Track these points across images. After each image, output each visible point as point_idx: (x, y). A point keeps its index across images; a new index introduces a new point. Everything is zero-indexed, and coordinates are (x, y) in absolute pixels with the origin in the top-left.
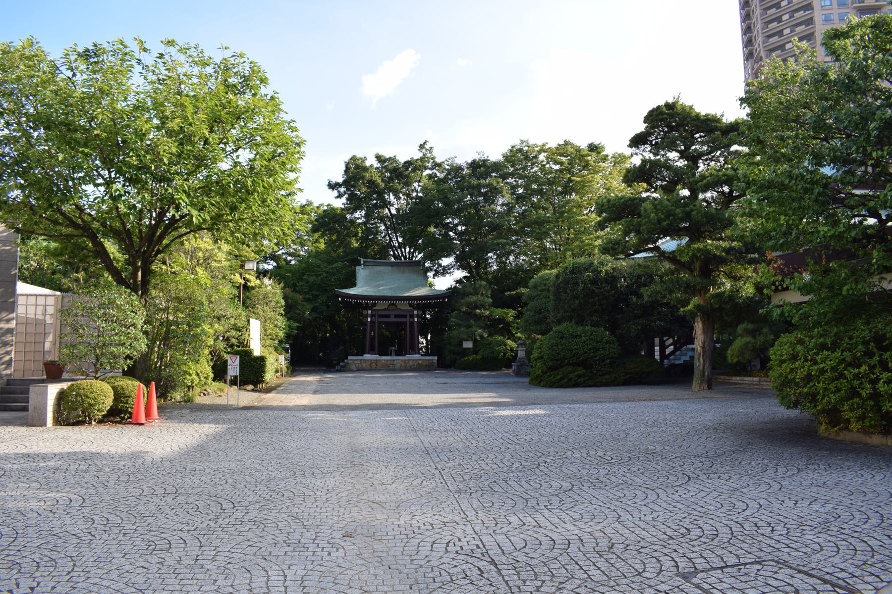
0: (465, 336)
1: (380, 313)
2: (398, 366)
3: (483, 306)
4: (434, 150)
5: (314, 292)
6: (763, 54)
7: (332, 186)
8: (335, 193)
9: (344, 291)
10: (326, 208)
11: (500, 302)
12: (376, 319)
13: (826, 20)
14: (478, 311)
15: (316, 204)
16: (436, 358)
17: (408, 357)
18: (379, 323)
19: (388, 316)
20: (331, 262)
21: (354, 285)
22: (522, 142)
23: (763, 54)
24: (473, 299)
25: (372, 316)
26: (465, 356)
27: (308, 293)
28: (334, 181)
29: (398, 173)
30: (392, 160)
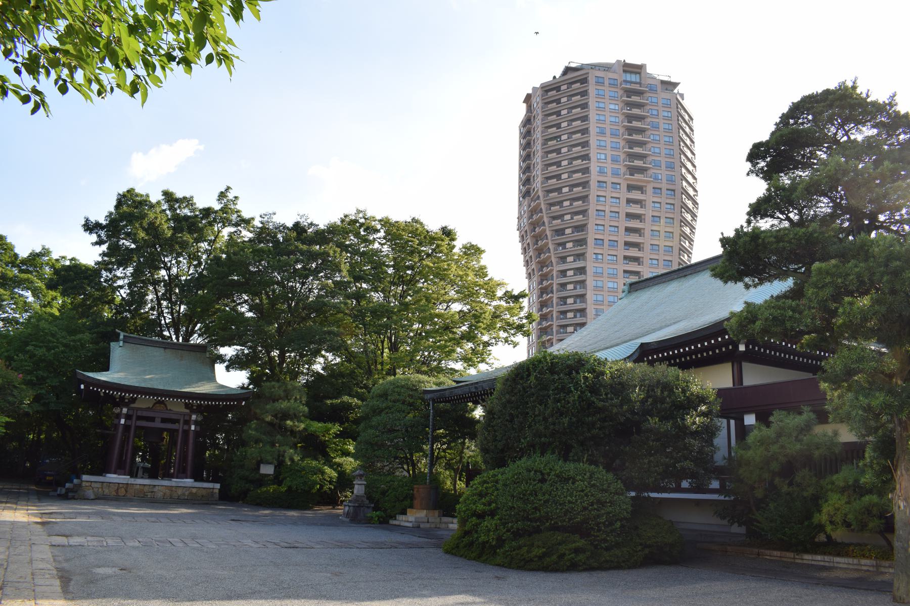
0: (269, 458)
1: (139, 413)
2: (160, 495)
3: (295, 417)
4: (239, 202)
5: (41, 373)
6: (540, 193)
7: (90, 227)
8: (94, 238)
9: (91, 375)
10: (68, 263)
11: (317, 414)
12: (133, 423)
13: (600, 172)
14: (289, 422)
15: (55, 256)
16: (218, 486)
17: (175, 482)
18: (137, 427)
19: (152, 419)
20: (72, 332)
21: (106, 368)
22: (359, 212)
23: (540, 193)
24: (284, 405)
25: (128, 417)
26: (261, 486)
27: (29, 373)
28: (93, 220)
29: (190, 224)
30: (187, 201)
